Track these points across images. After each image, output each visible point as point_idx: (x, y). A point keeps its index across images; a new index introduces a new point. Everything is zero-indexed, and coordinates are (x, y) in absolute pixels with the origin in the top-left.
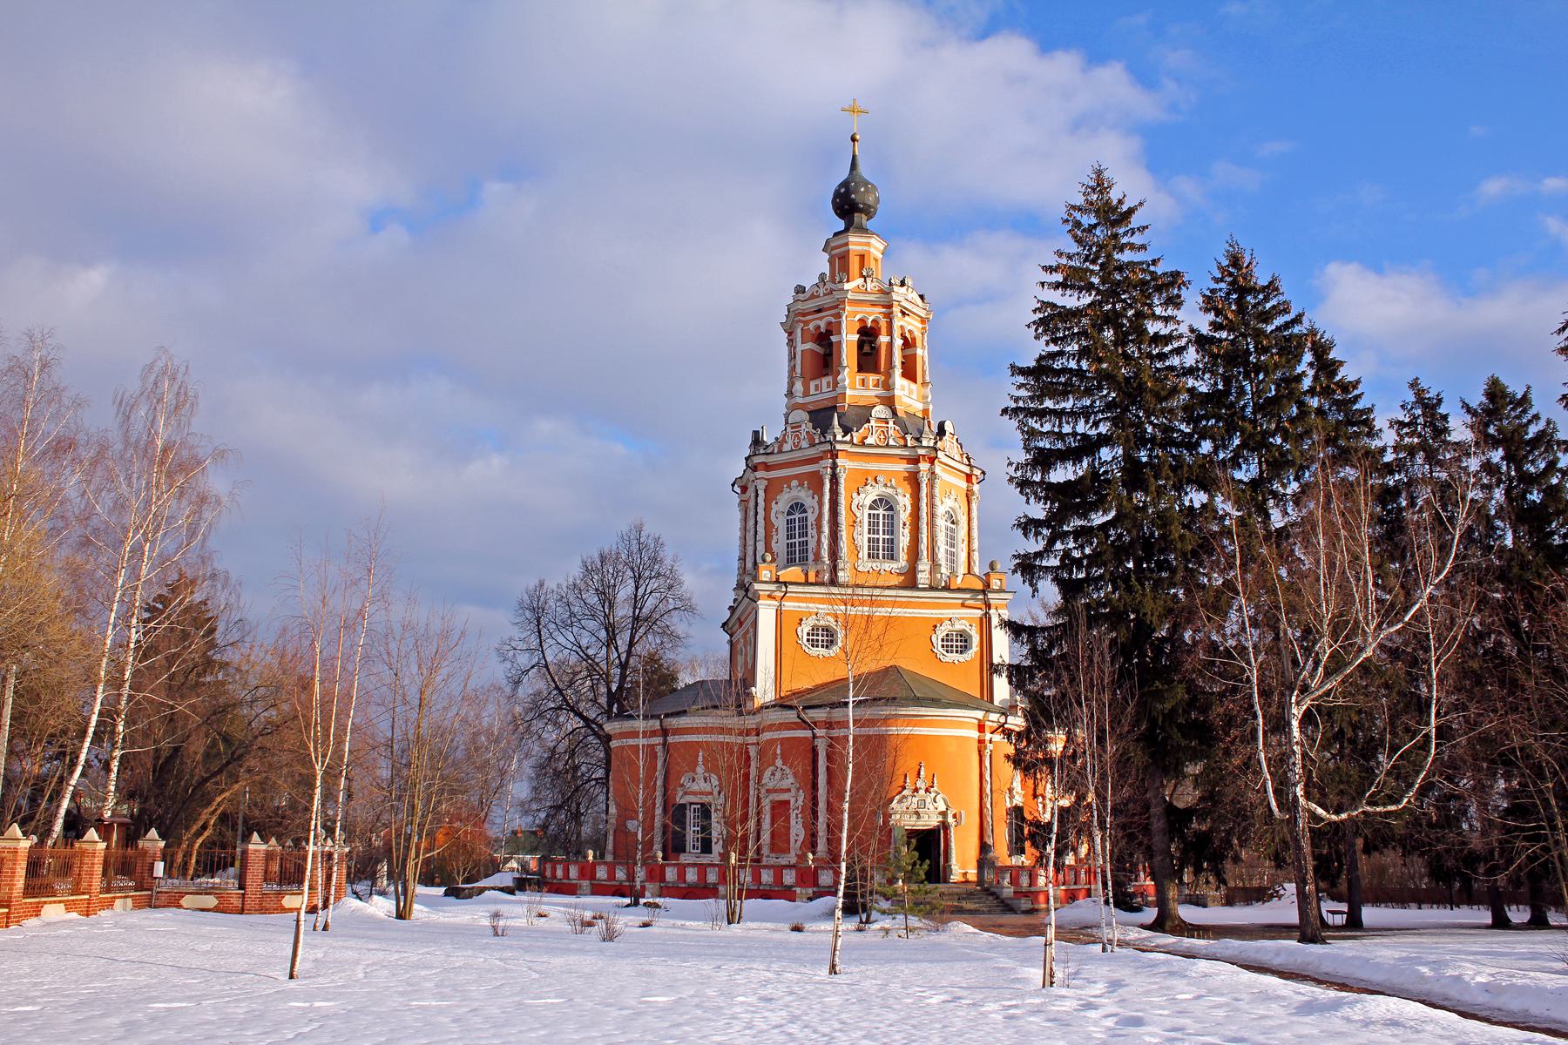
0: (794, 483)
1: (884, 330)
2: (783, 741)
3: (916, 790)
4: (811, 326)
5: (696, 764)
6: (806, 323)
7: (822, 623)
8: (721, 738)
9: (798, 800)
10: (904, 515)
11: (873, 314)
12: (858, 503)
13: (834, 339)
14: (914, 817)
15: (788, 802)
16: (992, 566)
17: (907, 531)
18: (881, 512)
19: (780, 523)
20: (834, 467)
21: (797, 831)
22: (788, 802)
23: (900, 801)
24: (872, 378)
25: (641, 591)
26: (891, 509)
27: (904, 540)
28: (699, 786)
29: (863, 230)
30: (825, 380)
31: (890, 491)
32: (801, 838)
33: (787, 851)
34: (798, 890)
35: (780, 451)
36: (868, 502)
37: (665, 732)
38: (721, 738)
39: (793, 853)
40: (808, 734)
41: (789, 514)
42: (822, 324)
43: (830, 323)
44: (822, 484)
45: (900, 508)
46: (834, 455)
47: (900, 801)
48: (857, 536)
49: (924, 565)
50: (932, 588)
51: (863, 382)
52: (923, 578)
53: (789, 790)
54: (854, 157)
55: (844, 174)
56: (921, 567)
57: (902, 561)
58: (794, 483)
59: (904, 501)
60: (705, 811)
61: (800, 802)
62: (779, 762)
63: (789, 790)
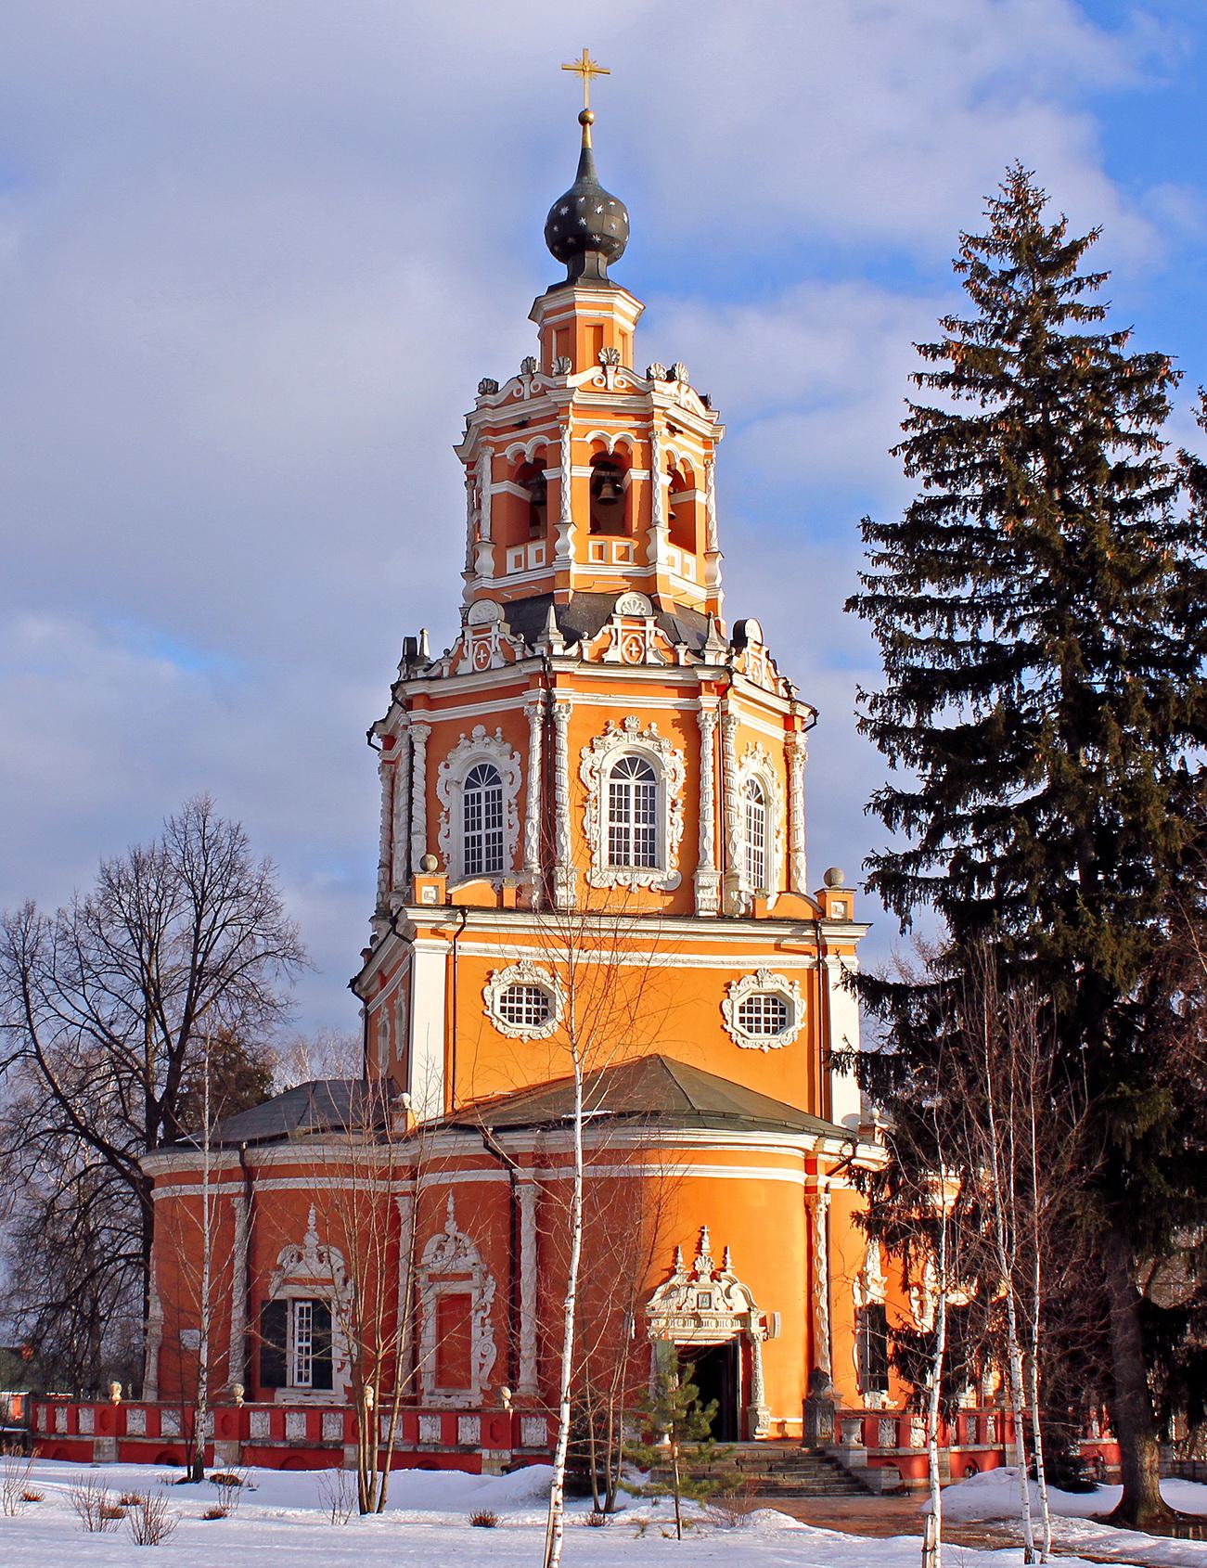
0: (479, 730)
1: (637, 458)
2: (459, 1188)
3: (695, 1276)
4: (508, 452)
5: (304, 1230)
6: (500, 446)
7: (527, 979)
8: (348, 1184)
9: (483, 1293)
10: (673, 788)
11: (618, 431)
12: (592, 766)
13: (548, 474)
14: (692, 1325)
15: (467, 1297)
16: (829, 878)
17: (678, 816)
18: (632, 781)
19: (453, 801)
20: (549, 701)
21: (484, 1349)
22: (467, 1297)
23: (666, 1296)
24: (616, 544)
25: (206, 923)
26: (650, 776)
27: (673, 831)
28: (309, 1268)
29: (600, 281)
30: (532, 548)
31: (648, 744)
32: (490, 1361)
33: (465, 1383)
34: (485, 1453)
35: (454, 675)
36: (609, 765)
37: (248, 1173)
38: (348, 1184)
39: (476, 1388)
40: (502, 1176)
41: (469, 785)
42: (528, 449)
43: (541, 447)
44: (527, 733)
45: (666, 775)
46: (549, 680)
47: (666, 1296)
48: (590, 826)
49: (708, 877)
50: (722, 917)
51: (601, 552)
52: (707, 899)
53: (469, 1276)
54: (584, 153)
55: (567, 183)
56: (702, 880)
57: (671, 869)
58: (479, 730)
59: (673, 763)
60: (320, 1314)
61: (489, 1297)
62: (451, 1227)
63: (469, 1276)
